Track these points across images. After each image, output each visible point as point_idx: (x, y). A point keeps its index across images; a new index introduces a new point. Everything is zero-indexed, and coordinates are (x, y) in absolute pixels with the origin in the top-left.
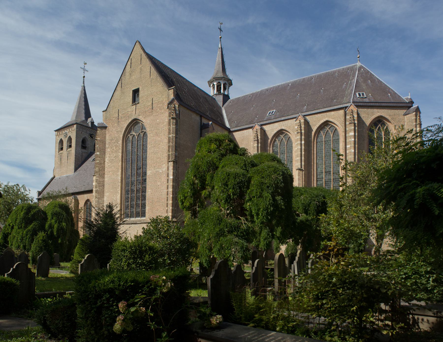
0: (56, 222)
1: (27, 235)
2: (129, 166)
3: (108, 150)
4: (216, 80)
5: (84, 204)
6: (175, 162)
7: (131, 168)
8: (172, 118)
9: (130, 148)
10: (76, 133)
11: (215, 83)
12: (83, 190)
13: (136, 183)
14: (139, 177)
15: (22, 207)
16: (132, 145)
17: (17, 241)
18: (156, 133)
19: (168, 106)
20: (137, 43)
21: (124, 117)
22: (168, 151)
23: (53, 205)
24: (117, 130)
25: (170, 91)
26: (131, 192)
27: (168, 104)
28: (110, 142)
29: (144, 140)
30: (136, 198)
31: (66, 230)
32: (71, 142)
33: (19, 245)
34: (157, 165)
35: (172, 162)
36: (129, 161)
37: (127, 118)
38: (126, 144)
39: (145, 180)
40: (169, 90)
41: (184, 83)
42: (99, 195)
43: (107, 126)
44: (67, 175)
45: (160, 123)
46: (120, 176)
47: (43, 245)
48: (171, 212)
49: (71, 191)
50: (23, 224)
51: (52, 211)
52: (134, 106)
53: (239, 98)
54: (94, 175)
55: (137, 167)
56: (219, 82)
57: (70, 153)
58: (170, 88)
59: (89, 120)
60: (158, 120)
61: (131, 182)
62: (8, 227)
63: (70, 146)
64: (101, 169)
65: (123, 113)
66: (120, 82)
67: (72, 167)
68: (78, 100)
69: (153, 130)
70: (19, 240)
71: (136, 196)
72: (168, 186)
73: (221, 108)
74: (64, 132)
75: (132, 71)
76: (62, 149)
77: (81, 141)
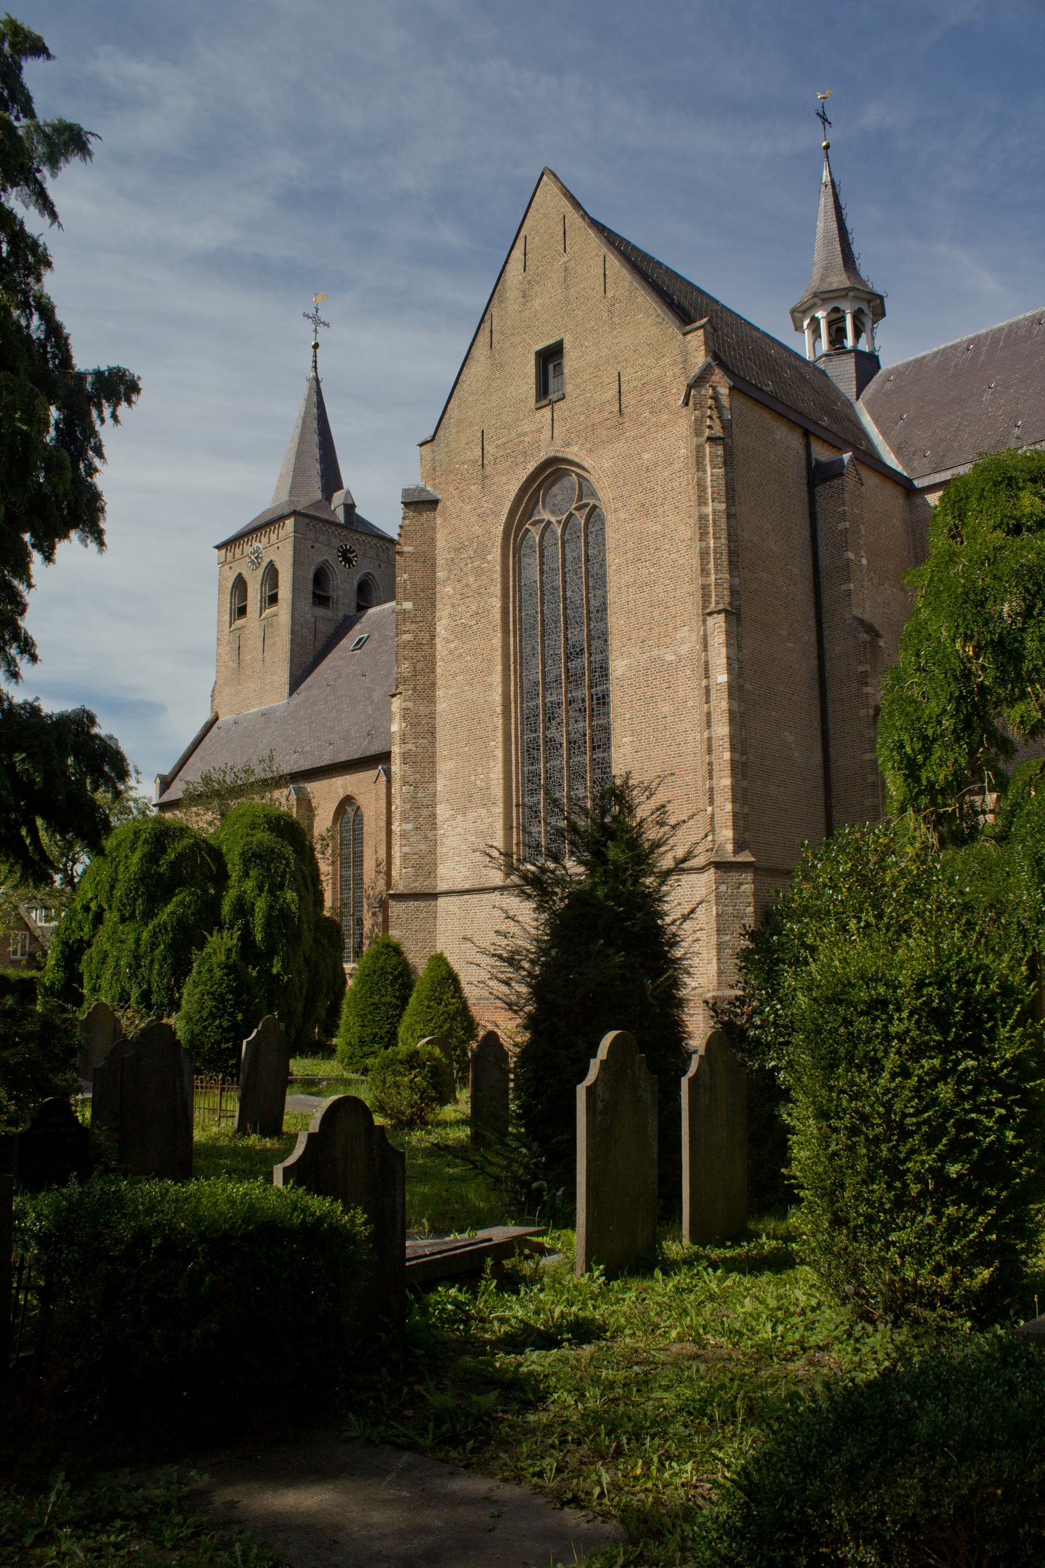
0: (260, 888)
1: (154, 946)
2: (533, 648)
3: (446, 591)
4: (823, 300)
5: (332, 814)
6: (733, 615)
7: (543, 655)
8: (710, 439)
9: (532, 572)
10: (295, 549)
11: (820, 314)
12: (326, 760)
13: (567, 712)
14: (577, 687)
15: (135, 833)
16: (542, 564)
17: (117, 972)
18: (643, 505)
19: (687, 396)
20: (545, 178)
21: (508, 455)
22: (702, 570)
23: (245, 820)
24: (478, 511)
25: (689, 337)
26: (545, 751)
27: (690, 387)
28: (453, 559)
29: (590, 539)
30: (569, 776)
31: (300, 920)
32: (275, 585)
33: (123, 989)
34: (655, 632)
35: (721, 618)
36: (534, 628)
37: (521, 459)
38: (518, 563)
39: (603, 700)
40: (685, 334)
41: (716, 314)
42: (415, 773)
43: (440, 497)
44: (264, 707)
45: (656, 465)
46: (500, 690)
47: (228, 986)
48: (730, 823)
49: (286, 769)
50: (140, 901)
51: (242, 842)
52: (547, 412)
53: (920, 362)
54: (394, 691)
55: (566, 648)
56: (836, 310)
57: (271, 625)
58: (688, 328)
59: (338, 498)
60: (646, 456)
61: (544, 710)
62: (80, 917)
63: (273, 599)
64: (419, 666)
65: (499, 442)
66: (486, 325)
67: (283, 676)
68: (298, 431)
69: (626, 493)
70: (123, 969)
71: (569, 767)
72: (709, 714)
73: (851, 404)
74: (248, 549)
75: (529, 282)
76: (242, 611)
77: (311, 576)
